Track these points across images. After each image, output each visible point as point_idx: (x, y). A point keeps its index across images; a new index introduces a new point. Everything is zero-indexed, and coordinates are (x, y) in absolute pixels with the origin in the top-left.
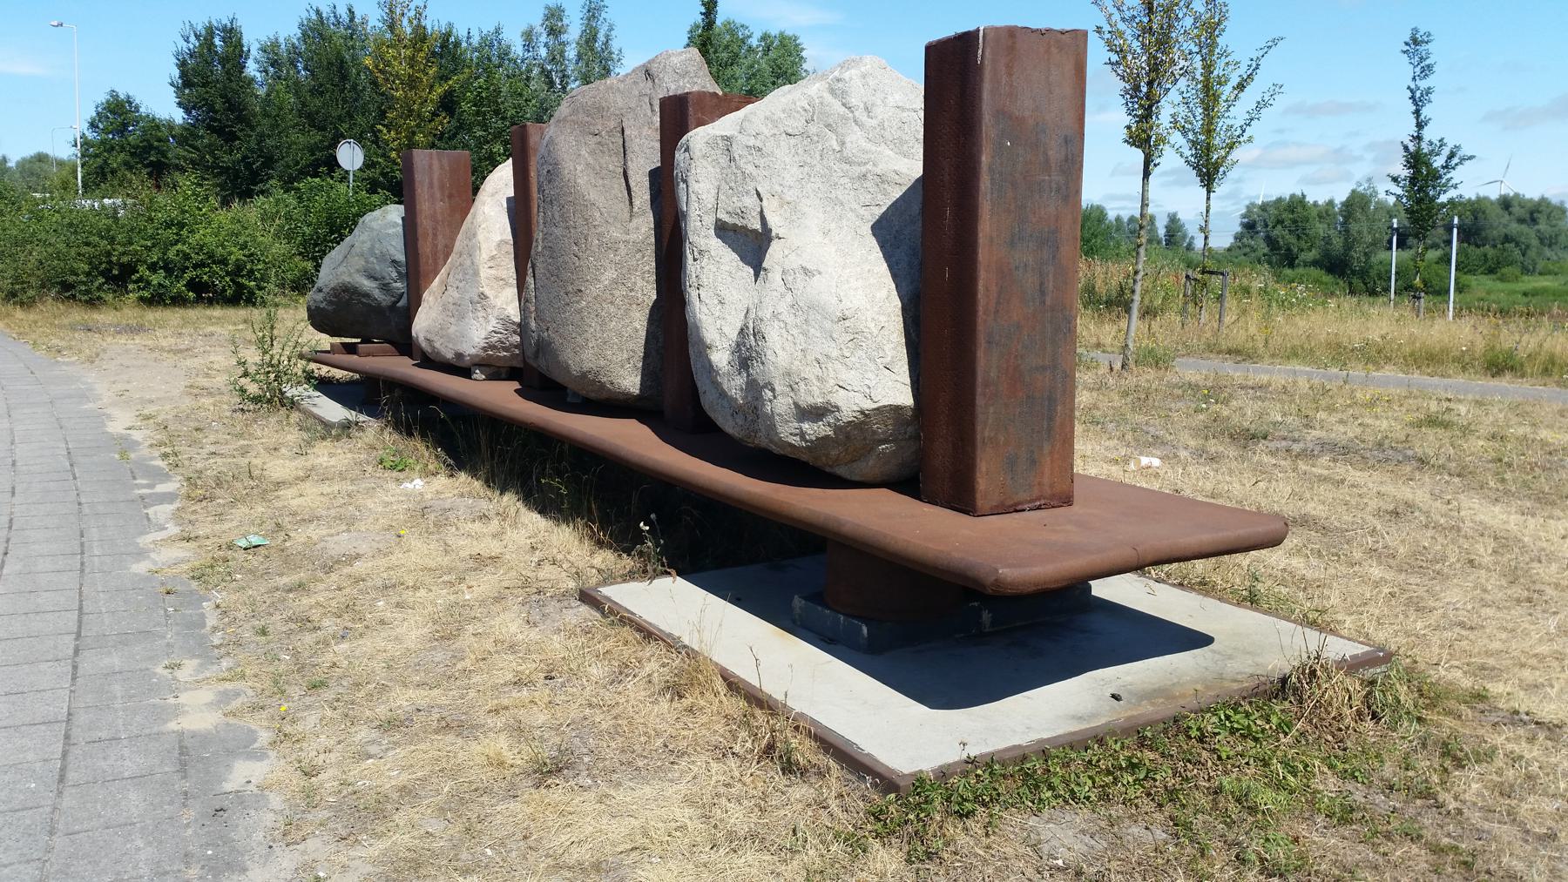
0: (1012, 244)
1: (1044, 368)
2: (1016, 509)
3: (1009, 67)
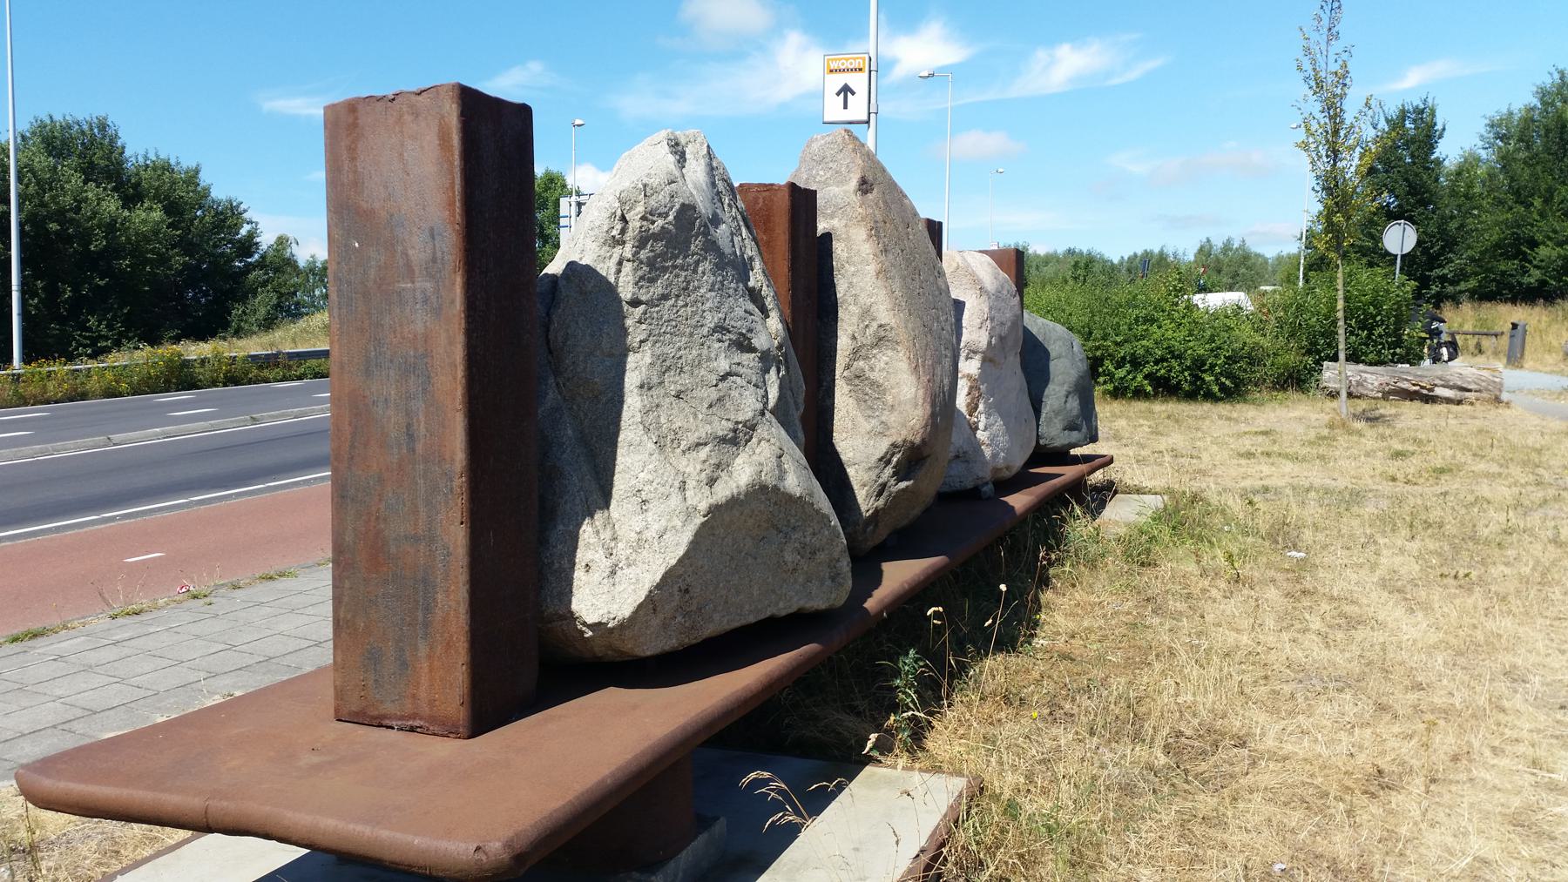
0: (368, 373)
1: (416, 539)
2: (379, 723)
3: (352, 150)
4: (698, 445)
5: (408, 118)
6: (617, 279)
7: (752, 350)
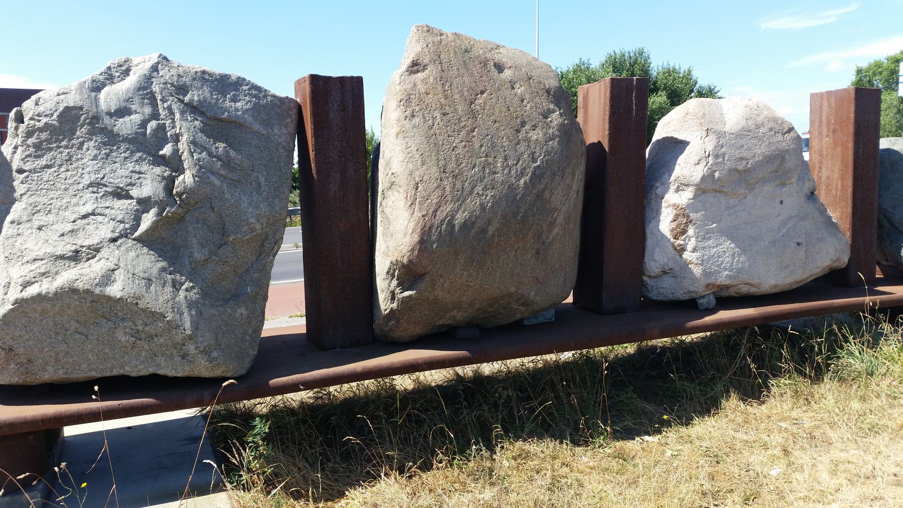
4: (35, 260)
6: (12, 158)
7: (132, 198)
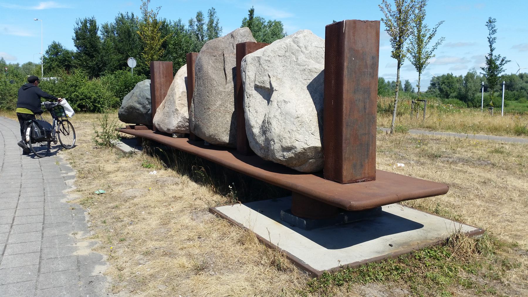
0: (355, 92)
1: (365, 134)
3: (354, 33)
5: (369, 28)
